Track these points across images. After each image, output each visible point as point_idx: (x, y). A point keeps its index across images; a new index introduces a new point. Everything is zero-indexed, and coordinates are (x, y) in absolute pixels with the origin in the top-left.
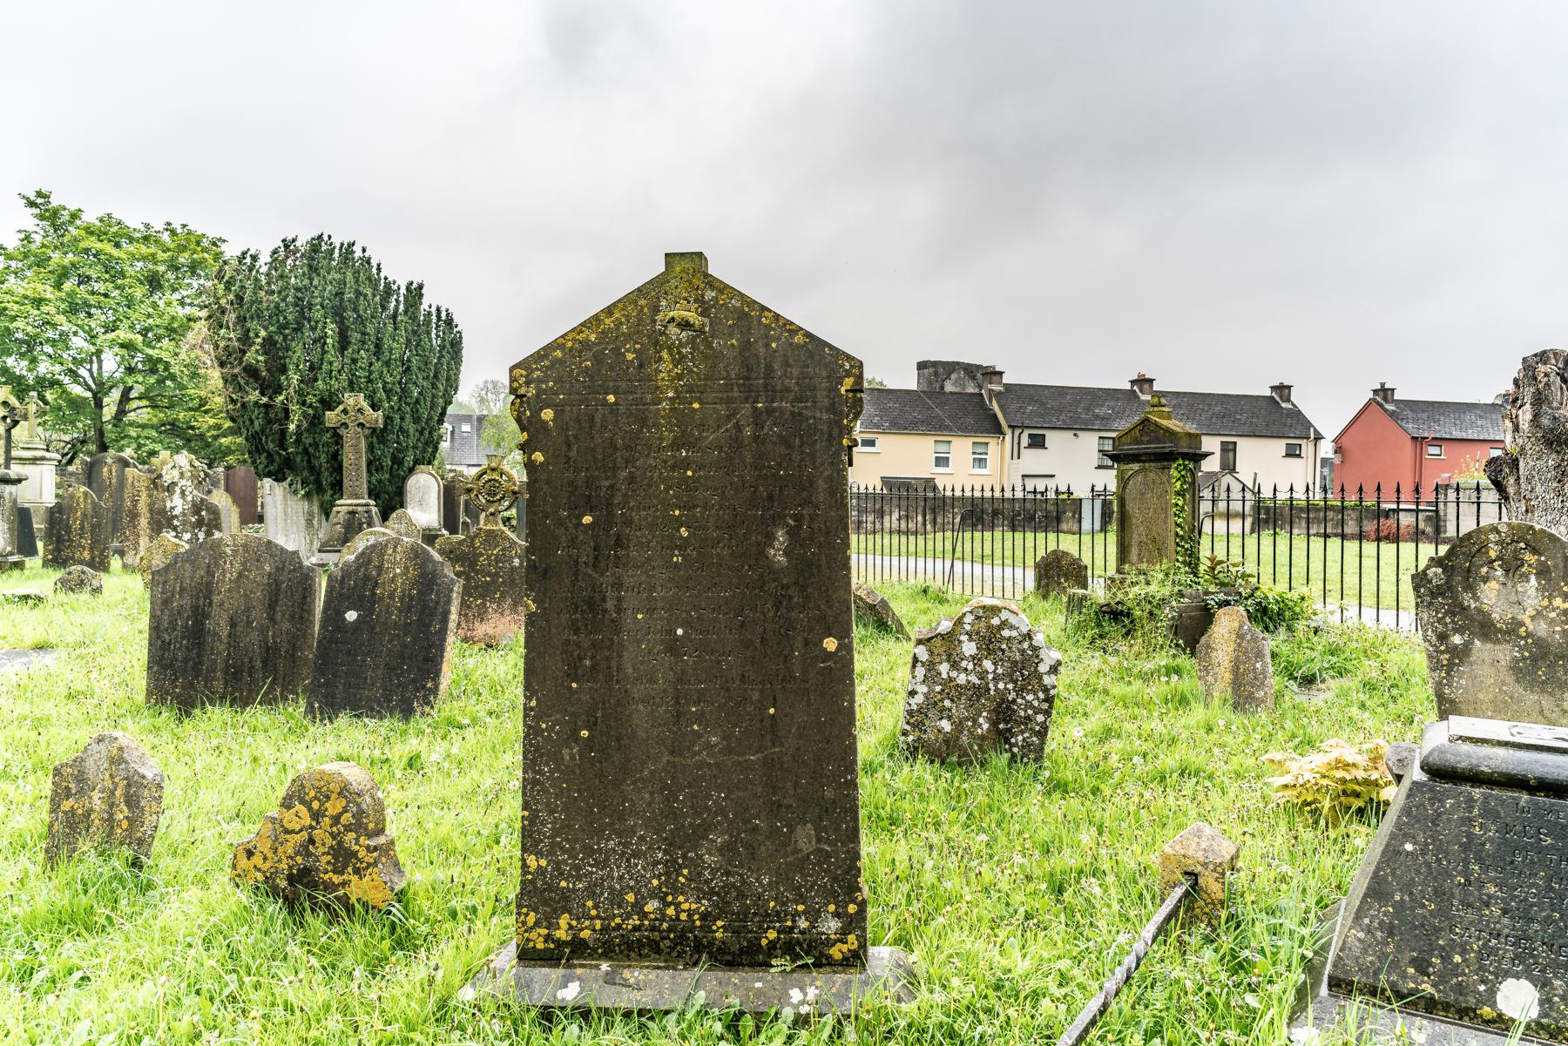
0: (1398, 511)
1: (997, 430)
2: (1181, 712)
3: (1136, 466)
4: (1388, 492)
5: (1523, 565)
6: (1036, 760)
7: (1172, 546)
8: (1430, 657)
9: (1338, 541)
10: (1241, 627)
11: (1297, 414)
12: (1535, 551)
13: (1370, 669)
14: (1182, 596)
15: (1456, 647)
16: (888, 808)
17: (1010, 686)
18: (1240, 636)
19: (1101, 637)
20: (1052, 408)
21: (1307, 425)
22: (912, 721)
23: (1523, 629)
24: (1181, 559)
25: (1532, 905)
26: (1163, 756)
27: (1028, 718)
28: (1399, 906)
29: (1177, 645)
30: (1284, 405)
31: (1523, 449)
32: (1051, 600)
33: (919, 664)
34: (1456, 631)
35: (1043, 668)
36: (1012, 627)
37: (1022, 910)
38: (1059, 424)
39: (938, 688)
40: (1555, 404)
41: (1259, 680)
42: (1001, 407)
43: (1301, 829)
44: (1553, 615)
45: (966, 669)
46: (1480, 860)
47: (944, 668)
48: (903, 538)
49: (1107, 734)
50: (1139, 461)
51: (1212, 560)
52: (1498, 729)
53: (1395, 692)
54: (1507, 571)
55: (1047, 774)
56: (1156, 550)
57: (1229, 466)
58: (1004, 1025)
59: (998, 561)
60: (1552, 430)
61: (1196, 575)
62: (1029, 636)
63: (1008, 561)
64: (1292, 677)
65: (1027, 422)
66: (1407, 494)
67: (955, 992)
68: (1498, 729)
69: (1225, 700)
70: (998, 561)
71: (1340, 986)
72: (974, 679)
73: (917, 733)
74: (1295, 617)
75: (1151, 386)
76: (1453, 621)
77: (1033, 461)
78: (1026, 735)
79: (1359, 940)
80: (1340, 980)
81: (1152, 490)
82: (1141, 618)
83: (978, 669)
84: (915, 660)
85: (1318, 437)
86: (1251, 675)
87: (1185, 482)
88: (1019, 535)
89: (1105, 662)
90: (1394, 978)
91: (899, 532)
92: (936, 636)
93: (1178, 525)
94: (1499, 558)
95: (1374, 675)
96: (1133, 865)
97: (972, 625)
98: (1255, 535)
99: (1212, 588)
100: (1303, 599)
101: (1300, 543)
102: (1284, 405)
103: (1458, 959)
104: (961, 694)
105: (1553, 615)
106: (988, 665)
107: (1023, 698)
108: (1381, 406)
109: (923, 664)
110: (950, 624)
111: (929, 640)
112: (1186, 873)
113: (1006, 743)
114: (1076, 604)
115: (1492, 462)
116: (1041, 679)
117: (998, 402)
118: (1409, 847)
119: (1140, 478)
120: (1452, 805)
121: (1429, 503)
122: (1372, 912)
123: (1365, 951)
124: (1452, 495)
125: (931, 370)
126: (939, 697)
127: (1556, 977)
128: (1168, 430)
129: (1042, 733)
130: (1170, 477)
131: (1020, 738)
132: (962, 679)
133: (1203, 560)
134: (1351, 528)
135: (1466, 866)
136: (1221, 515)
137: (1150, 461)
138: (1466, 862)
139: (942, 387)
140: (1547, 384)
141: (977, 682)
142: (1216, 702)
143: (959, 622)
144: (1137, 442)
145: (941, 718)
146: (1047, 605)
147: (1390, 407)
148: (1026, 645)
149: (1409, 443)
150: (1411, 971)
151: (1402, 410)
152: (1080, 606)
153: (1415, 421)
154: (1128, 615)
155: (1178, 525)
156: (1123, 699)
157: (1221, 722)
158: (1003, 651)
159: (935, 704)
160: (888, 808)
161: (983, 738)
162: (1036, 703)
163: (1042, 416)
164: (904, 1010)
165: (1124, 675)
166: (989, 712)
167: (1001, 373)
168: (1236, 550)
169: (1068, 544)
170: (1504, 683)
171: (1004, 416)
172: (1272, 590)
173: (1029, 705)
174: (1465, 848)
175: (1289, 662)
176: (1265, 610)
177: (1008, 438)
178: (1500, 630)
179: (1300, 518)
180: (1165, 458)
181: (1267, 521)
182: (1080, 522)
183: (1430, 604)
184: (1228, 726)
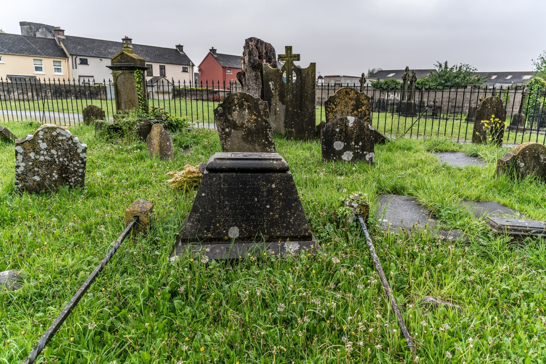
0: (219, 91)
1: (64, 56)
2: (7, 144)
3: (120, 72)
4: (216, 85)
5: (244, 106)
6: (81, 187)
7: (137, 103)
8: (220, 136)
9: (201, 101)
10: (161, 131)
11: (185, 56)
12: (247, 101)
13: (205, 142)
14: (141, 121)
15: (227, 132)
16: (9, 216)
17: (65, 159)
18: (161, 134)
19: (111, 138)
20: (89, 48)
21: (189, 61)
22: (19, 178)
23: (244, 126)
24: (141, 108)
25: (237, 205)
26: (133, 178)
27: (76, 171)
28: (201, 213)
29: (141, 139)
30: (181, 53)
31: (246, 69)
32: (90, 125)
33: (19, 154)
34: (227, 127)
35: (79, 151)
36: (62, 135)
37: (73, 242)
38: (93, 55)
39: (31, 163)
40: (254, 55)
41: (169, 148)
42: (65, 46)
43: (178, 195)
44: (252, 121)
45: (43, 154)
46: (223, 195)
47: (32, 155)
48: (22, 103)
49: (113, 172)
50: (121, 70)
51: (153, 107)
52: (240, 155)
53: (212, 148)
54: (240, 108)
55: (86, 191)
56: (131, 104)
57: (163, 74)
58: (64, 285)
59: (71, 111)
60: (254, 64)
61: (147, 113)
62: (71, 138)
63: (75, 111)
64: (181, 147)
65: (78, 53)
66: (221, 85)
67: (41, 279)
68: (240, 155)
69: (158, 157)
70: (71, 111)
71: (184, 241)
72: (48, 158)
73: (23, 183)
74: (182, 127)
75: (131, 42)
76: (226, 124)
77: (82, 70)
78: (76, 177)
79: (190, 226)
80: (185, 239)
81: (128, 81)
82: (126, 130)
83: (49, 153)
84: (17, 153)
85: (193, 65)
86: (166, 147)
87: (140, 78)
88: (79, 101)
89: (112, 147)
90: (200, 235)
91: (19, 100)
92: (26, 141)
93: (139, 95)
94: (237, 104)
95: (206, 144)
96: (117, 217)
97: (43, 135)
98: (174, 100)
99: (152, 118)
100: (184, 120)
101: (189, 102)
102: (181, 53)
103: (218, 225)
104: (42, 165)
105: (252, 121)
106: (53, 151)
107: (72, 163)
108: (212, 55)
109: (21, 154)
110: (32, 136)
111: (22, 143)
112: (135, 217)
113: (67, 182)
114: (99, 126)
115: (239, 73)
116: (79, 155)
117: (63, 44)
118: (203, 195)
119: (122, 76)
120: (215, 180)
121: (228, 89)
122: (193, 217)
123: (192, 229)
124: (234, 86)
125: (28, 26)
126: (32, 167)
127: (243, 224)
128: (131, 58)
129: (83, 176)
130: (134, 76)
131: (73, 179)
132: (42, 158)
133: (150, 108)
134: (205, 97)
135: (219, 197)
136: (161, 93)
137: (126, 70)
138: (219, 196)
139: (35, 35)
140: (252, 49)
141: (49, 159)
142: (154, 158)
143: (37, 135)
144: (120, 62)
145: (35, 175)
146: (89, 127)
147: (215, 56)
148: (70, 142)
149: (221, 68)
150: (205, 231)
151: (219, 57)
152: (101, 127)
153: (223, 61)
154: (121, 129)
155: (139, 95)
156: (120, 160)
157: (155, 164)
158: (60, 146)
159: (30, 170)
160: (9, 216)
161: (56, 181)
162: (78, 165)
163: (85, 51)
164: (16, 293)
165: (119, 151)
166: (57, 171)
167: (63, 31)
168: (167, 105)
169: (96, 103)
170: (240, 143)
171: (67, 50)
172: (174, 117)
173: (75, 166)
174: (219, 192)
175: (180, 142)
176: (172, 125)
177: (70, 59)
178: (239, 126)
179: (189, 94)
180: (131, 69)
181: (177, 95)
182: (106, 94)
183: (219, 119)
184: (158, 165)
